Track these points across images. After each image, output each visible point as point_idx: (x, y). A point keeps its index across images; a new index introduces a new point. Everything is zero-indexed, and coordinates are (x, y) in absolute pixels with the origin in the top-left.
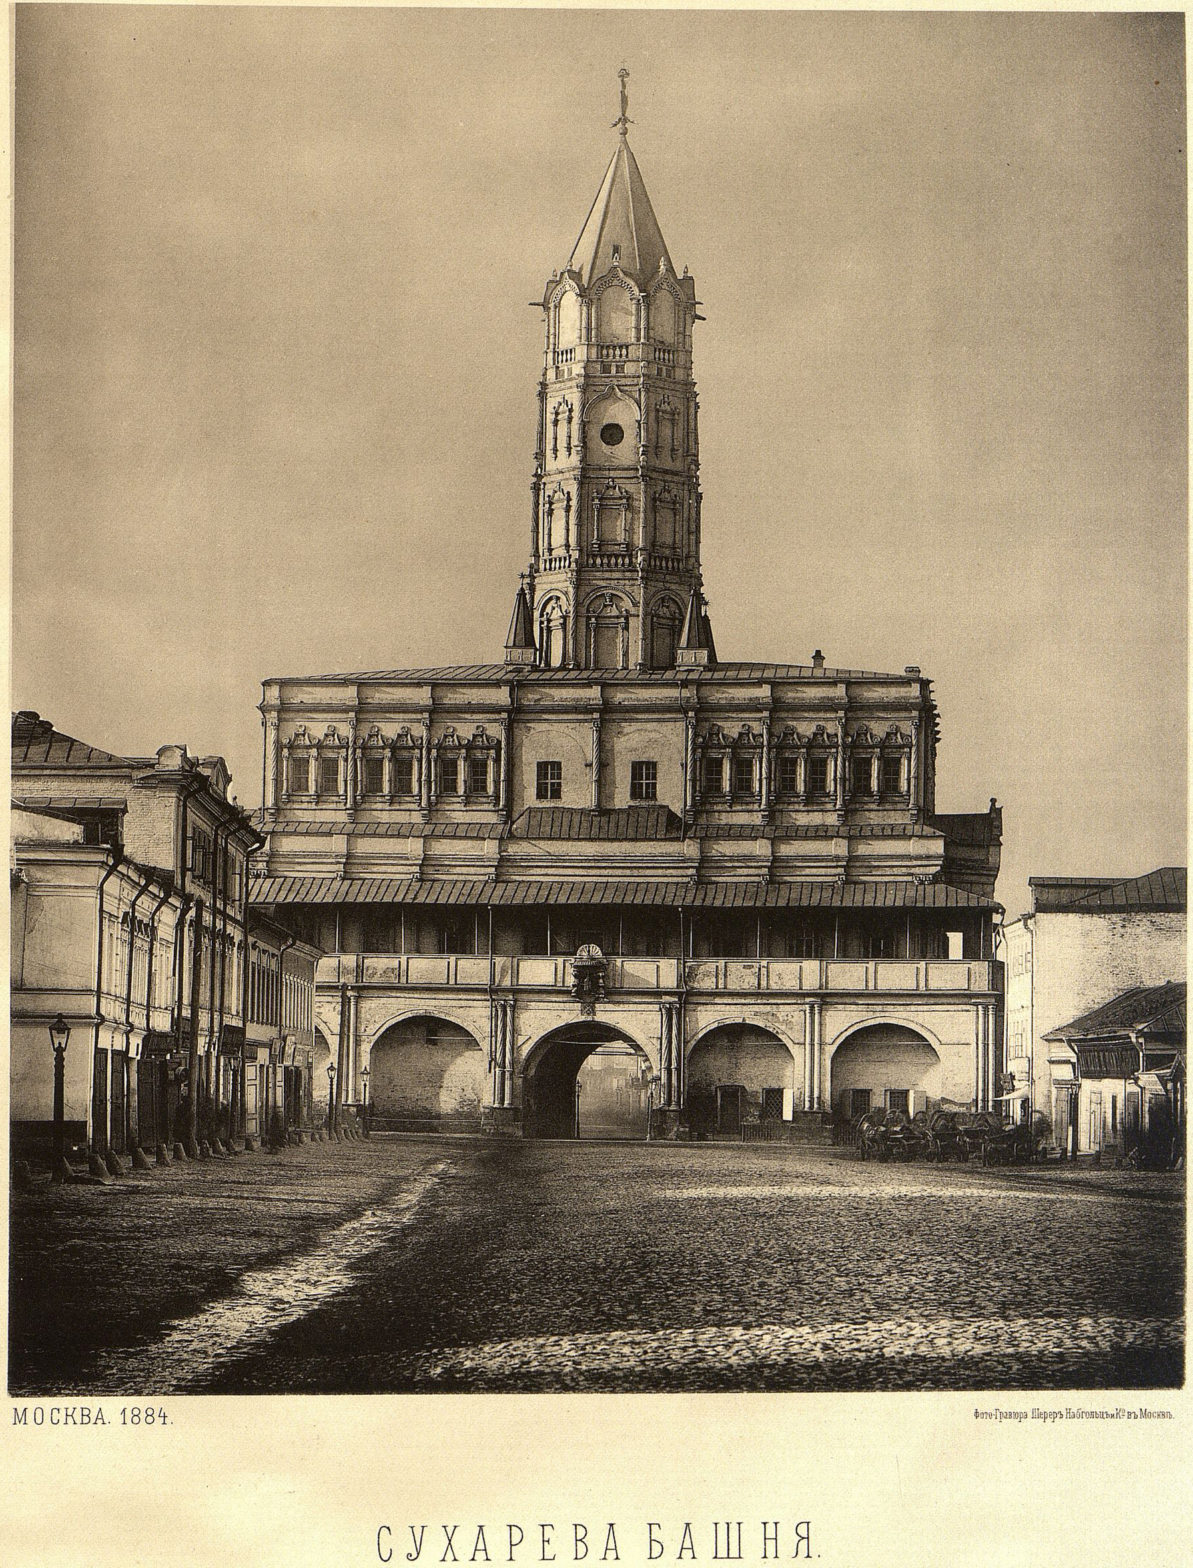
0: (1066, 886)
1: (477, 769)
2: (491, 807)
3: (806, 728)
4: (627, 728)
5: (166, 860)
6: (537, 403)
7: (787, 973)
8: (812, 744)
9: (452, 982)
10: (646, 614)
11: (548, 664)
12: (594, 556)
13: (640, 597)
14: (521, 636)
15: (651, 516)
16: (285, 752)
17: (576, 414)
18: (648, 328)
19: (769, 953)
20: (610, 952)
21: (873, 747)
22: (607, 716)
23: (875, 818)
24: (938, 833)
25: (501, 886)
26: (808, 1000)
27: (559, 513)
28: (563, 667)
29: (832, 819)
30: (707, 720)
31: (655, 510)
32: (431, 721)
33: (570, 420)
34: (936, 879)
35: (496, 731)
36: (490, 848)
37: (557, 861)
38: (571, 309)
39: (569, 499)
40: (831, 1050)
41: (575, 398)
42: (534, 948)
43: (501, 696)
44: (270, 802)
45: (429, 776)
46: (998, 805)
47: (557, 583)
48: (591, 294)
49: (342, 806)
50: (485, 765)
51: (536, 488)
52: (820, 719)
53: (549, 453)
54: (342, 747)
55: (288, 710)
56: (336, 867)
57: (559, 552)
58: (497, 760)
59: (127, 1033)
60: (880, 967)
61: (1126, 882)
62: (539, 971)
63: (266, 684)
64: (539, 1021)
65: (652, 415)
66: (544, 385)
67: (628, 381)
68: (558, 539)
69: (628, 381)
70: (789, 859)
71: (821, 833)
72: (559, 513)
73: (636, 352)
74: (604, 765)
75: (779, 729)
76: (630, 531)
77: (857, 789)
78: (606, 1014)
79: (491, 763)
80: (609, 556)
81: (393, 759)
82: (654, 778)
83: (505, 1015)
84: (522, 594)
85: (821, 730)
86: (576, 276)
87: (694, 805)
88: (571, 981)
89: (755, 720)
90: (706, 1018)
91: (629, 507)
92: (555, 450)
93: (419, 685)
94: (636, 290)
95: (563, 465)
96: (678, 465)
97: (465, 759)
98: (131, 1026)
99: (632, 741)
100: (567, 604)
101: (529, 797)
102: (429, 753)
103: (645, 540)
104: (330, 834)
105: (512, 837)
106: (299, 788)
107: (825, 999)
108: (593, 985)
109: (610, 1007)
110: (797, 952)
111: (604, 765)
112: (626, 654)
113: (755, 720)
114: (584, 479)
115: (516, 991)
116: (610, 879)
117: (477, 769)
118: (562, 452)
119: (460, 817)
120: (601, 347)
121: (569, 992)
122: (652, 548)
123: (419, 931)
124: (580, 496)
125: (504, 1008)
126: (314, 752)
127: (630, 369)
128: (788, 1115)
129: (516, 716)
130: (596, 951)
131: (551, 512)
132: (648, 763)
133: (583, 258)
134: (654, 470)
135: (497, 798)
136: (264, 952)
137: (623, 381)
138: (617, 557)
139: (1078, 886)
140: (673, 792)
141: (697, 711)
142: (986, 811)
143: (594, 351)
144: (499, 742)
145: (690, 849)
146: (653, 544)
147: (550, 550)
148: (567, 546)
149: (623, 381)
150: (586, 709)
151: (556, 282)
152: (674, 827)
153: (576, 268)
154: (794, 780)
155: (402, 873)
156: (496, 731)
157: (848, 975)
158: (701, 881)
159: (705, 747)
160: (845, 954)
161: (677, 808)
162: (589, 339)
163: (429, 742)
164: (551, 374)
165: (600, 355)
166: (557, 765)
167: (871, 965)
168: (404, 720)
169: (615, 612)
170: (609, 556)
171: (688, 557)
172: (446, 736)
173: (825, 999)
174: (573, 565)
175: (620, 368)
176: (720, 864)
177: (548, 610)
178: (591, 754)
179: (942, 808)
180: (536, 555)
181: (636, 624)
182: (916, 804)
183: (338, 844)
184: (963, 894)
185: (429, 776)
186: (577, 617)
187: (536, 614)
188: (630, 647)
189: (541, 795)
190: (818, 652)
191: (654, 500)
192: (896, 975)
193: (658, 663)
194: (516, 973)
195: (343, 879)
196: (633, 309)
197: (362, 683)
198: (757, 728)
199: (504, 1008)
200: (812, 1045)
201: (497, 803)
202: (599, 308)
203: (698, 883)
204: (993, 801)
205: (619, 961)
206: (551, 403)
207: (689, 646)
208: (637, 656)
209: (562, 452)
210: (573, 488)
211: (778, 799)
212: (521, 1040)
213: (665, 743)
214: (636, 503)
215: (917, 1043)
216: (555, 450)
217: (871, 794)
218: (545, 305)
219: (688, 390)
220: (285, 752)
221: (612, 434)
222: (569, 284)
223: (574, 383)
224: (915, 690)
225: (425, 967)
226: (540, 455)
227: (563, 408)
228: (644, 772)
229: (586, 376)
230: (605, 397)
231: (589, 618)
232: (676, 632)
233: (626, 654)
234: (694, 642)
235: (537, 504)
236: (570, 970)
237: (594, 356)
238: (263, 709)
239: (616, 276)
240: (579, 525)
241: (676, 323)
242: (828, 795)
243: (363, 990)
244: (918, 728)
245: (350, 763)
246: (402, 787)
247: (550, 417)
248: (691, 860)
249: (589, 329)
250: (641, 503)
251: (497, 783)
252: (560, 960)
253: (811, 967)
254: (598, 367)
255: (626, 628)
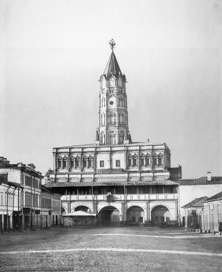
0: (186, 180)
1: (90, 162)
2: (92, 169)
3: (145, 153)
4: (115, 154)
5: (18, 181)
6: (99, 97)
7: (143, 196)
8: (146, 156)
9: (139, 199)
10: (118, 134)
11: (102, 143)
12: (109, 124)
13: (117, 132)
14: (97, 139)
15: (119, 117)
16: (57, 160)
17: (105, 100)
18: (117, 84)
19: (140, 193)
20: (113, 193)
21: (157, 156)
22: (112, 152)
23: (157, 169)
24: (168, 171)
25: (82, 183)
26: (146, 201)
27: (103, 117)
28: (104, 144)
29: (137, 170)
30: (154, 152)
31: (119, 116)
32: (69, 155)
33: (104, 101)
34: (168, 179)
35: (93, 155)
36: (92, 176)
37: (103, 178)
38: (104, 81)
39: (105, 115)
40: (150, 210)
41: (105, 97)
42: (100, 193)
43: (93, 149)
44: (55, 169)
45: (69, 164)
46: (180, 166)
47: (103, 129)
48: (108, 78)
49: (67, 169)
50: (136, 160)
51: (99, 113)
52: (65, 154)
53: (101, 107)
54: (162, 156)
55: (128, 151)
56: (66, 180)
57: (103, 124)
58: (93, 161)
59: (7, 211)
60: (167, 195)
61: (195, 180)
62: (100, 197)
63: (54, 148)
64: (101, 206)
65: (118, 99)
66: (100, 95)
67: (114, 94)
68: (103, 122)
69: (114, 94)
70: (143, 176)
71: (148, 172)
72: (103, 117)
73: (115, 89)
74: (111, 161)
75: (141, 154)
76: (115, 120)
77: (154, 164)
78: (112, 204)
79: (92, 161)
80: (112, 124)
81: (158, 158)
82: (120, 162)
83: (95, 205)
84: (97, 131)
85: (148, 154)
86: (105, 76)
87: (126, 168)
88: (106, 199)
89: (136, 152)
90: (129, 205)
91: (115, 116)
92: (102, 106)
93: (67, 148)
94: (115, 77)
95: (104, 110)
96: (123, 108)
97: (75, 161)
98: (8, 210)
99: (116, 157)
100: (105, 133)
101: (99, 167)
102: (81, 159)
103: (118, 121)
104: (65, 174)
105: (96, 174)
106: (90, 166)
107: (150, 201)
108: (110, 199)
109: (113, 203)
110: (145, 192)
111: (111, 161)
112: (115, 141)
113: (136, 152)
114: (107, 111)
115: (97, 201)
116: (119, 181)
117: (90, 162)
118: (103, 106)
119: (74, 171)
120: (109, 88)
121: (106, 201)
122: (119, 123)
123: (81, 192)
124: (107, 114)
125: (95, 204)
126: (62, 160)
127: (114, 91)
128: (144, 222)
129: (96, 153)
130: (110, 194)
131: (102, 117)
132: (103, 161)
133: (106, 73)
134: (119, 109)
135: (93, 167)
136: (47, 196)
137: (113, 94)
138: (113, 124)
139: (188, 180)
140: (123, 166)
141: (127, 151)
142: (178, 167)
143: (108, 88)
144: (93, 157)
145: (126, 175)
146: (119, 122)
147: (102, 123)
148: (105, 123)
149: (113, 94)
150: (108, 151)
151: (101, 77)
152: (123, 171)
153: (105, 74)
154: (143, 162)
155: (150, 179)
156: (93, 155)
157: (153, 196)
158: (128, 181)
159: (128, 157)
160: (153, 193)
161: (124, 168)
162: (107, 86)
163: (81, 158)
164: (101, 93)
165: (109, 89)
166: (103, 161)
167: (157, 195)
168: (65, 154)
169: (113, 134)
170: (112, 124)
171: (126, 124)
172: (129, 155)
173: (150, 201)
174: (106, 126)
175: (113, 92)
176: (71, 179)
177: (102, 134)
178: (109, 159)
179: (172, 167)
180: (100, 125)
181: (117, 136)
182: (165, 166)
183: (67, 176)
184: (173, 182)
185: (69, 164)
186: (107, 135)
187: (100, 135)
188: (116, 140)
189: (101, 166)
190: (148, 139)
191: (119, 114)
192: (162, 196)
193: (120, 143)
194: (97, 198)
195: (68, 182)
196: (115, 81)
197: (70, 149)
198: (137, 154)
199: (95, 204)
200: (147, 209)
201: (93, 168)
202: (109, 81)
203: (128, 181)
204: (179, 165)
205: (114, 195)
206: (101, 98)
207: (126, 140)
208: (117, 142)
209: (103, 106)
210: (105, 113)
211: (141, 165)
212: (98, 209)
213: (121, 157)
214: (116, 115)
215: (166, 209)
216: (102, 106)
217: (157, 165)
218: (100, 81)
219: (125, 95)
220: (57, 160)
221: (112, 103)
222: (104, 77)
223: (105, 94)
224: (163, 147)
225: (82, 197)
226: (100, 107)
227: (103, 99)
228: (118, 162)
229: (107, 93)
230: (110, 97)
231: (108, 135)
232: (123, 137)
233: (115, 141)
234: (127, 139)
235: (100, 116)
236: (106, 197)
237: (108, 90)
238: (54, 153)
239: (112, 75)
240: (107, 119)
241: (122, 83)
242: (149, 165)
243: (71, 201)
244: (164, 153)
245: (68, 162)
246: (64, 166)
247: (101, 100)
248: (92, 178)
249: (107, 85)
250: (117, 115)
251: (93, 165)
252: (104, 195)
253: (147, 195)
254: (109, 91)
255: (115, 137)
